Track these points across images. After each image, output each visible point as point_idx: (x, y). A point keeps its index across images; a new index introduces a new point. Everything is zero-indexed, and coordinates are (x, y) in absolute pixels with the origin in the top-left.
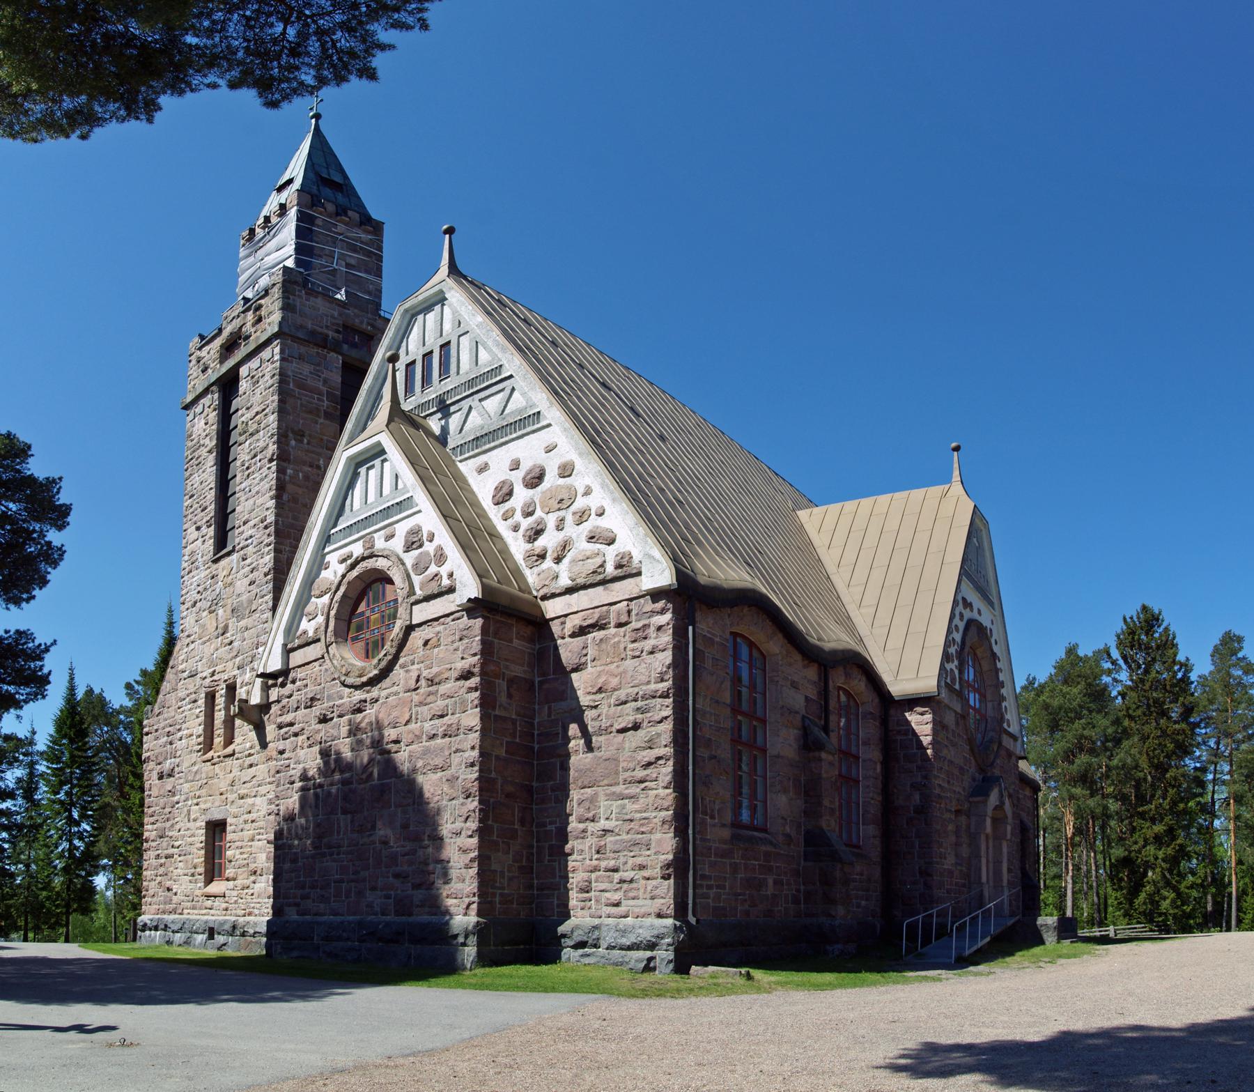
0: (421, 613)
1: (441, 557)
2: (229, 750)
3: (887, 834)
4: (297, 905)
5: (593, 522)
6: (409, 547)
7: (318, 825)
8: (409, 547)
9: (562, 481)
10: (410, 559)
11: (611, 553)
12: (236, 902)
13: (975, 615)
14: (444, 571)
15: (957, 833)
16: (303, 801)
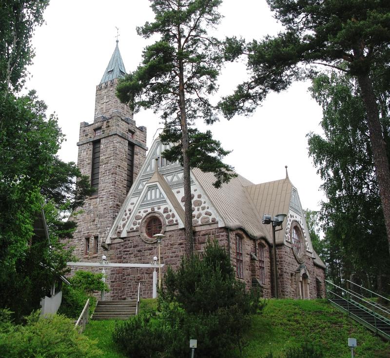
0: (168, 229)
1: (173, 216)
2: (96, 255)
3: (272, 281)
5: (206, 210)
6: (165, 212)
8: (165, 212)
9: (198, 199)
10: (165, 215)
11: (211, 218)
13: (295, 219)
14: (174, 219)
15: (370, 278)
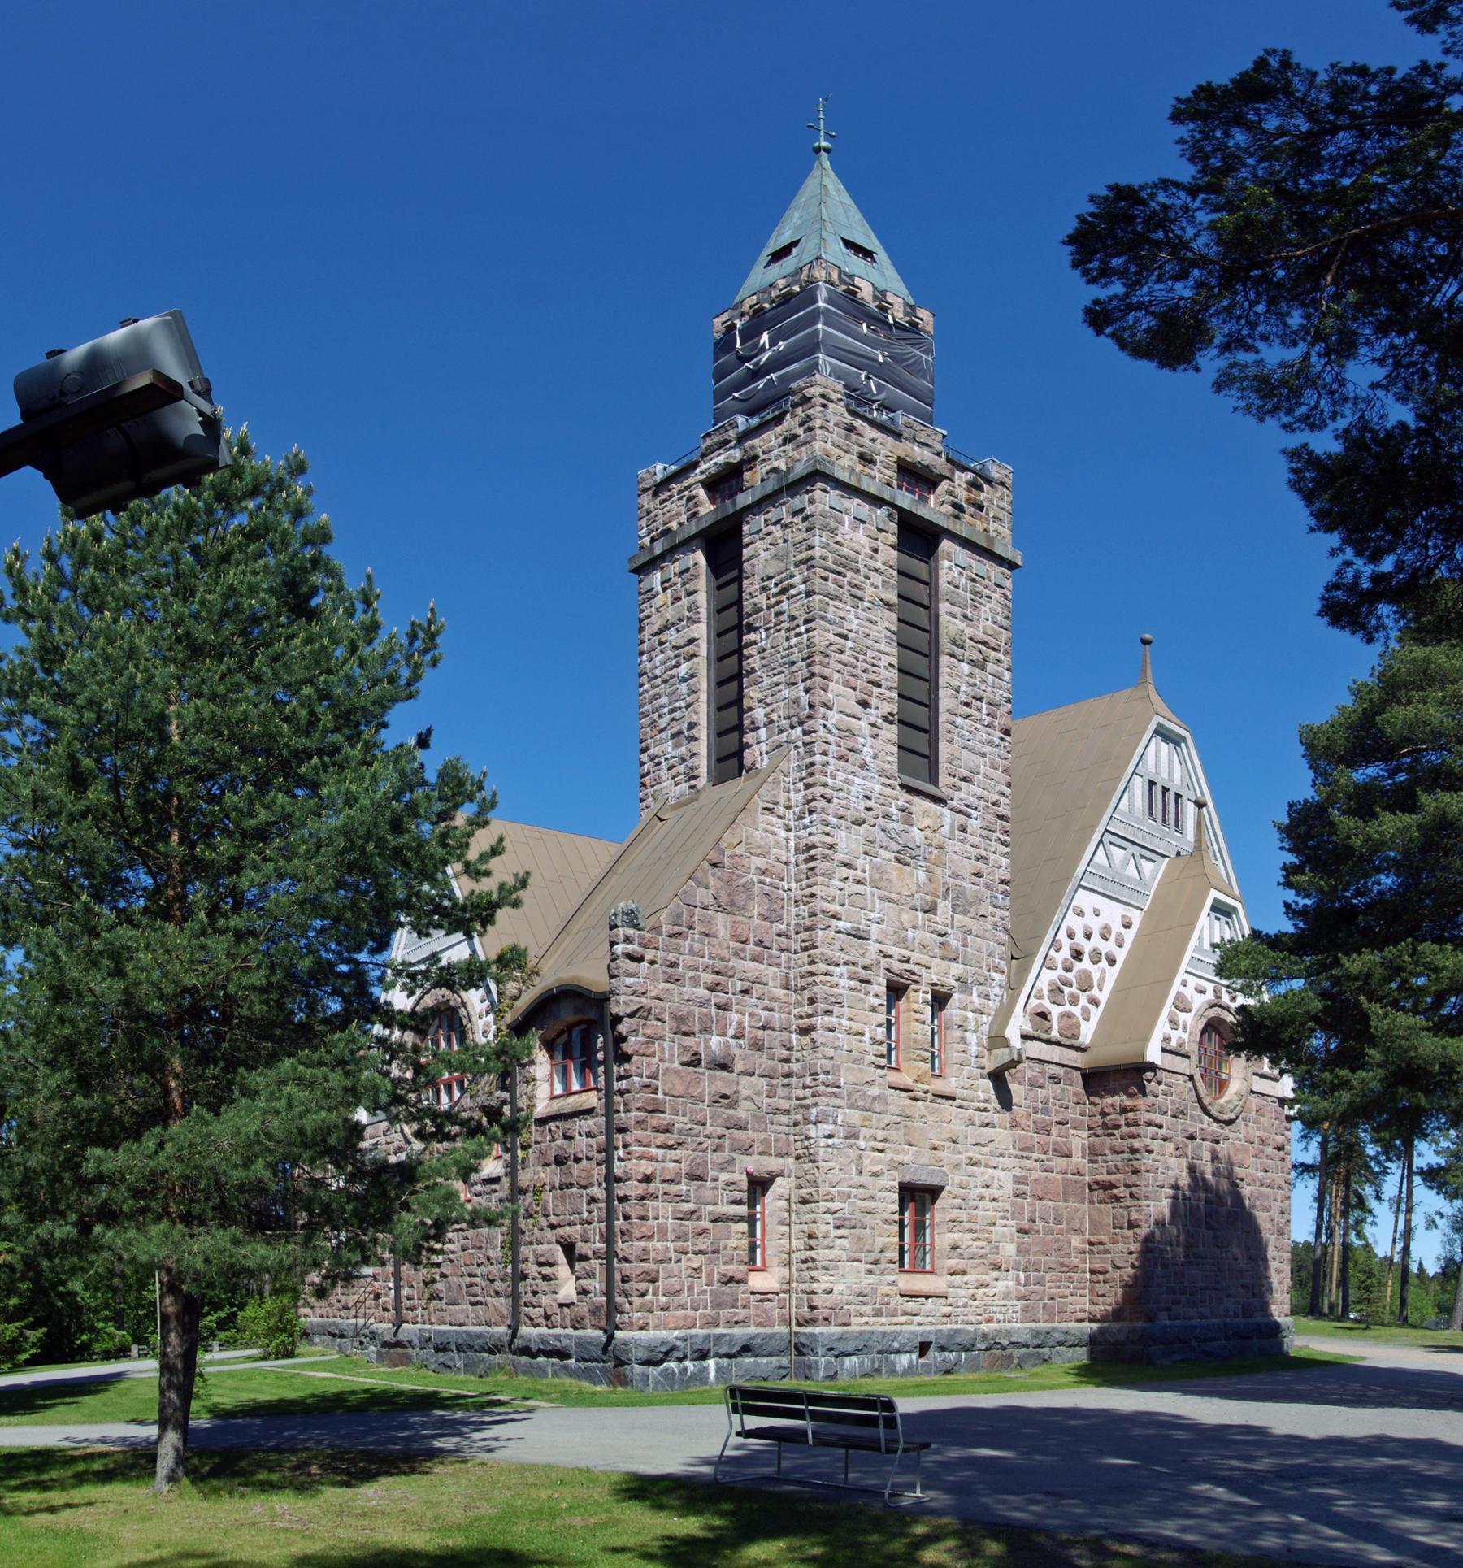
4: (1169, 1309)
7: (1188, 1234)
12: (965, 1306)
16: (1174, 1208)
